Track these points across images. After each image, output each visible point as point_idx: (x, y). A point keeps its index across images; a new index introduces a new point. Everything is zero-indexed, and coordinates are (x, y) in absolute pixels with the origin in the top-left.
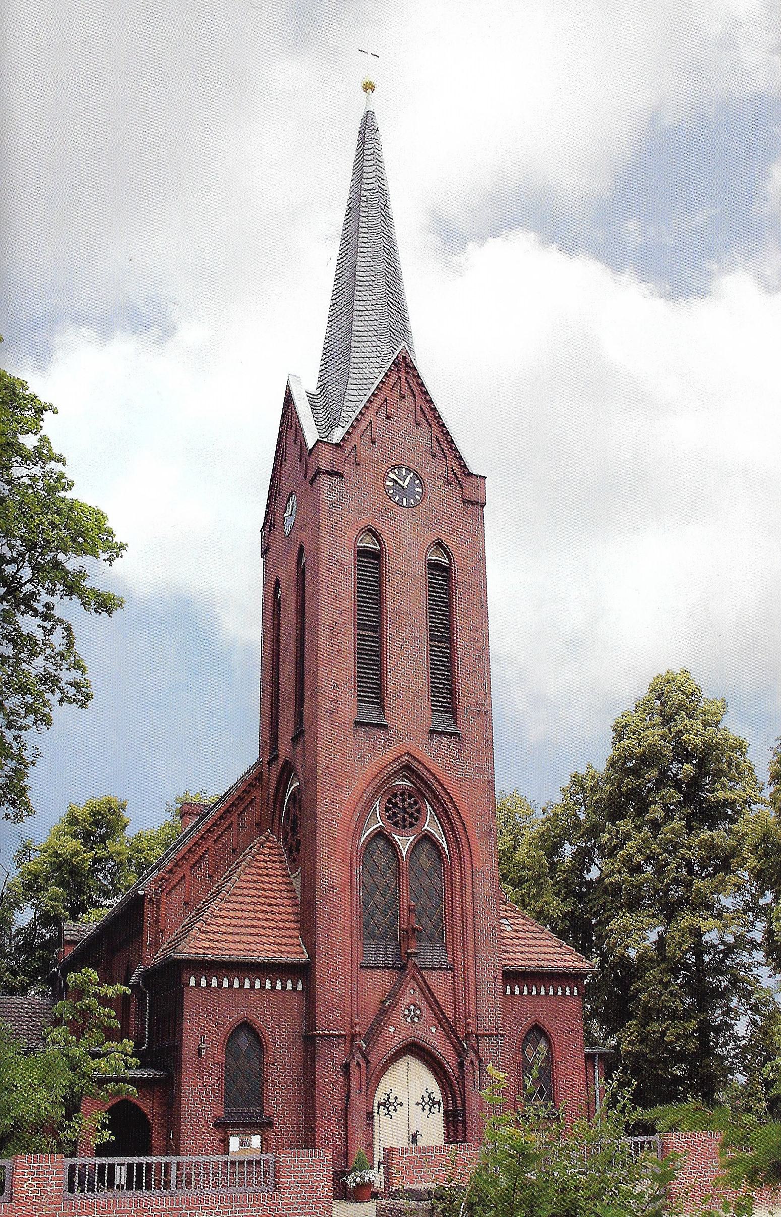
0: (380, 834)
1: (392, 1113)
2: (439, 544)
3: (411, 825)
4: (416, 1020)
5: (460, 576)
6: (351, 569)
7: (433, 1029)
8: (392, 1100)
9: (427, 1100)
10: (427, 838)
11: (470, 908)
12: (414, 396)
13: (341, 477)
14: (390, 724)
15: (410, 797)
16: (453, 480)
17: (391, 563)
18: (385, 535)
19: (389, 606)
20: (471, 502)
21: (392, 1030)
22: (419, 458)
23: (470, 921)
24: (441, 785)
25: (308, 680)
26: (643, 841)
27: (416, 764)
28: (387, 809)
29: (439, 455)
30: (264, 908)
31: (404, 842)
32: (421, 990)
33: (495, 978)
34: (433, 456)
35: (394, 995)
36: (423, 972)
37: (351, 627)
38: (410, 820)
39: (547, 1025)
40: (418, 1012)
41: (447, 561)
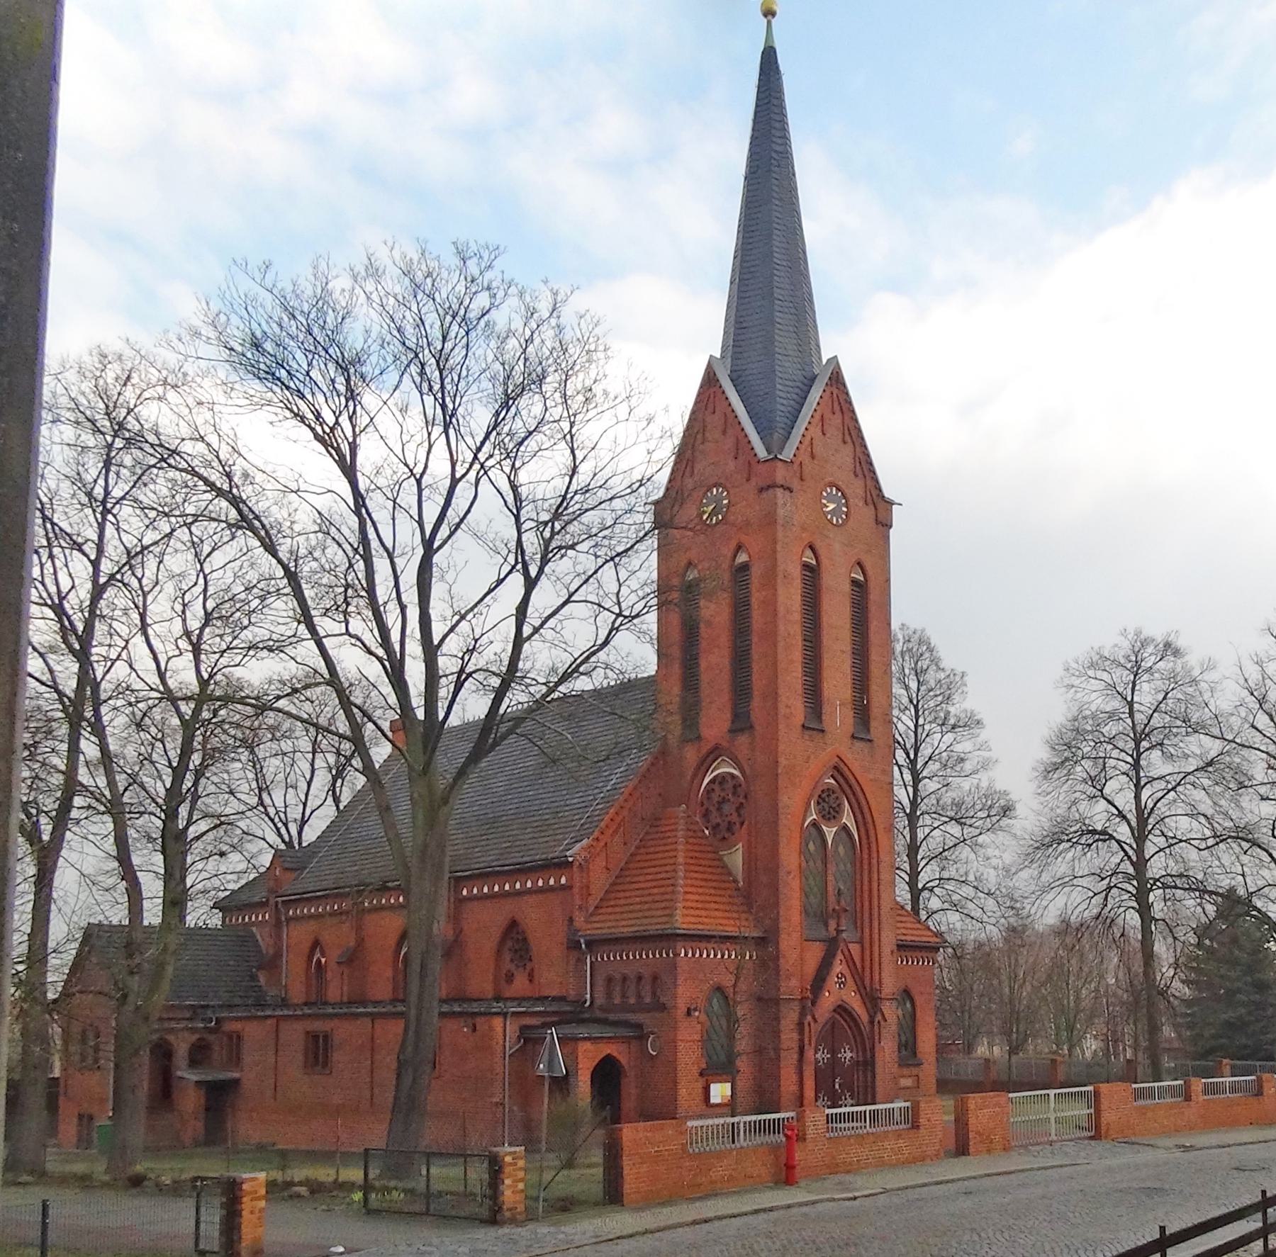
0: (814, 824)
2: (859, 564)
5: (874, 596)
11: (877, 977)
14: (826, 729)
18: (822, 552)
19: (825, 625)
21: (827, 994)
22: (844, 475)
23: (875, 876)
25: (757, 651)
29: (861, 476)
31: (830, 832)
38: (831, 814)
39: (914, 993)
41: (862, 579)
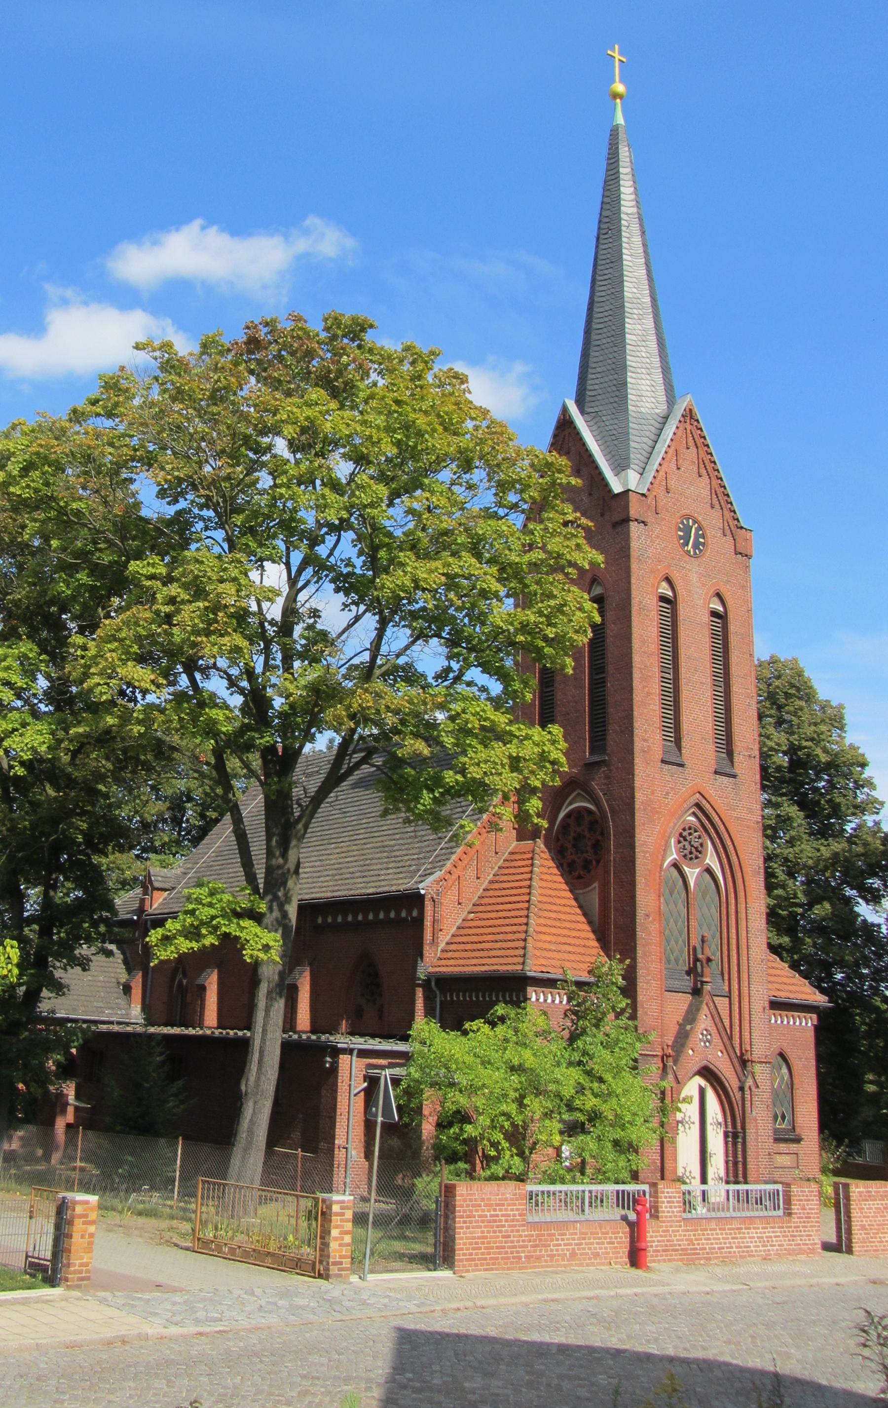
1: (687, 1130)
3: (697, 858)
4: (707, 1044)
6: (654, 614)
7: (720, 1054)
8: (687, 1119)
9: (687, 1126)
10: (709, 871)
12: (697, 447)
13: (646, 525)
15: (696, 831)
16: (728, 533)
17: (683, 611)
20: (740, 553)
21: (690, 1052)
24: (724, 824)
26: (515, 691)
27: (704, 802)
28: (679, 842)
29: (717, 506)
30: (568, 925)
31: (692, 873)
32: (712, 1016)
33: (764, 1009)
34: (712, 507)
35: (691, 1016)
36: (715, 998)
37: (656, 670)
40: (709, 1037)
